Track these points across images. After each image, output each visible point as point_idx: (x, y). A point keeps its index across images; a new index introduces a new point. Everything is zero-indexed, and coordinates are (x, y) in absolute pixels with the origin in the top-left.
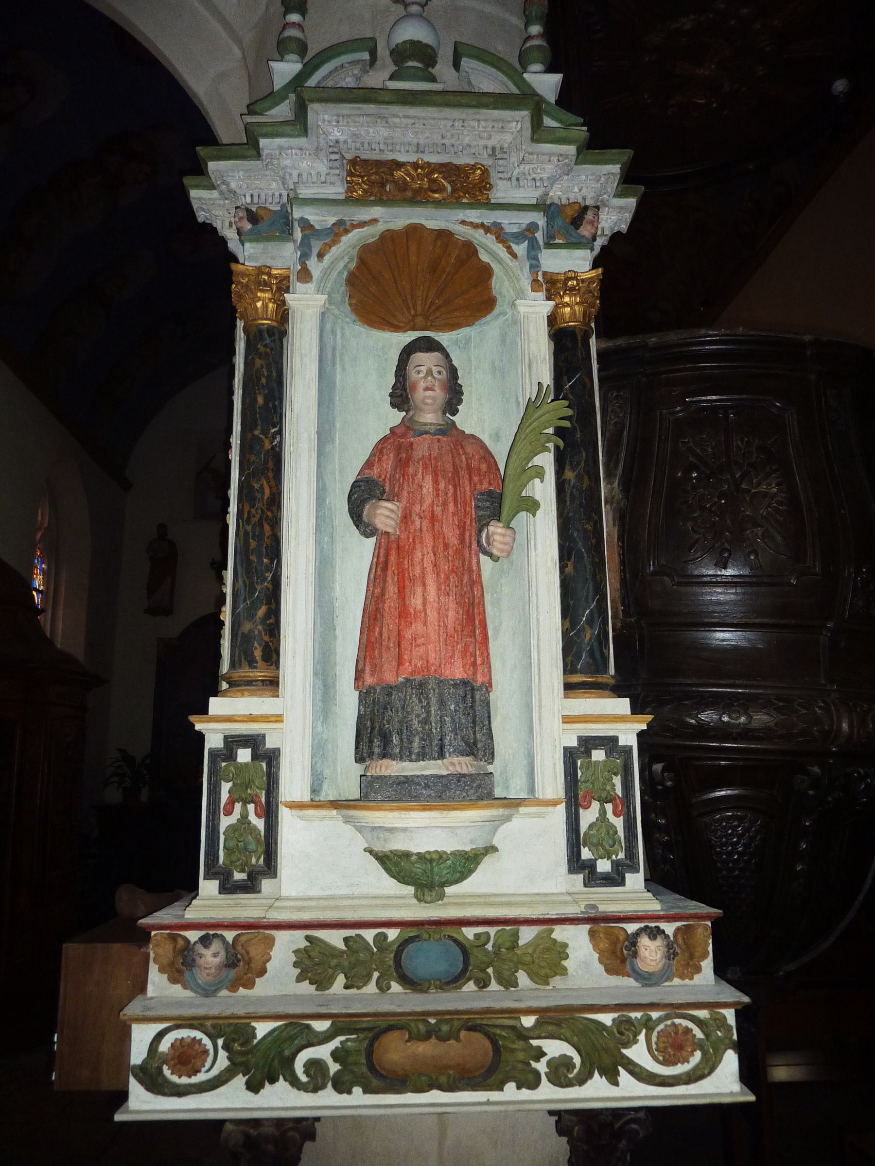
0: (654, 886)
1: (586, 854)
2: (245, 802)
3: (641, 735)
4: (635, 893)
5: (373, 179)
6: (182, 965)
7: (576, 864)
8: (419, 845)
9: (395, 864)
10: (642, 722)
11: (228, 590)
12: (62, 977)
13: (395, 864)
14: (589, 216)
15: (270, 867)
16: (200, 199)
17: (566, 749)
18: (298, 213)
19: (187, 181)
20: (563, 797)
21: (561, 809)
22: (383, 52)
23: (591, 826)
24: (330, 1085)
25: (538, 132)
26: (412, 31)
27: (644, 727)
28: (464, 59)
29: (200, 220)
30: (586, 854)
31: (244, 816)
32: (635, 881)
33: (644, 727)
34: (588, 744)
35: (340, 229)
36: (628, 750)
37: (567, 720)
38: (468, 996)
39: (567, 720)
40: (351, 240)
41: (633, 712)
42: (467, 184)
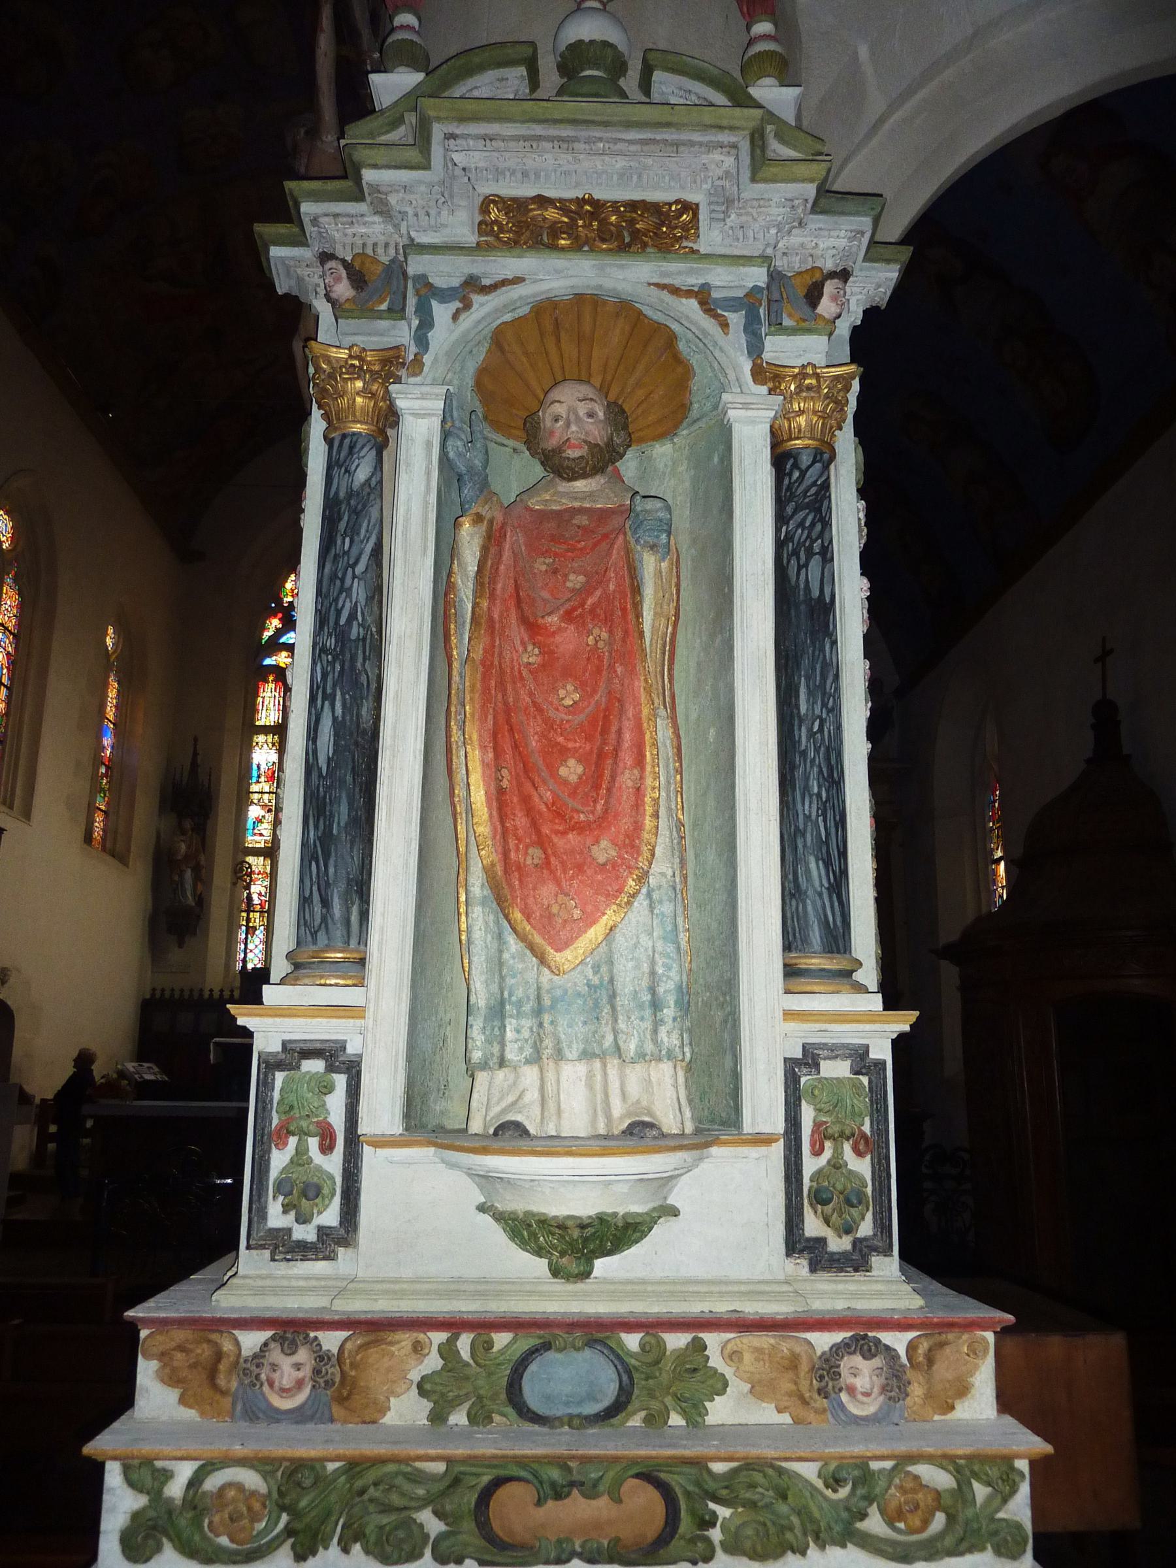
0: (907, 1266)
1: (813, 1226)
2: (303, 1133)
3: (900, 1044)
4: (887, 1286)
5: (520, 224)
6: (210, 1376)
7: (796, 1242)
8: (559, 1207)
9: (527, 1230)
10: (904, 1022)
11: (110, 713)
12: (197, 1315)
13: (527, 1230)
14: (829, 287)
15: (346, 1232)
16: (282, 259)
17: (300, 1557)
18: (415, 266)
19: (263, 229)
20: (782, 1132)
21: (778, 1148)
22: (548, 65)
23: (916, 1478)
24: (428, 1552)
25: (761, 165)
26: (589, 29)
27: (907, 1028)
28: (655, 73)
29: (282, 288)
30: (813, 1226)
31: (301, 1151)
32: (888, 1266)
33: (907, 1028)
34: (810, 1058)
35: (473, 285)
36: (881, 1064)
37: (789, 1015)
38: (629, 1439)
39: (789, 1015)
40: (484, 306)
41: (887, 1007)
42: (654, 228)
